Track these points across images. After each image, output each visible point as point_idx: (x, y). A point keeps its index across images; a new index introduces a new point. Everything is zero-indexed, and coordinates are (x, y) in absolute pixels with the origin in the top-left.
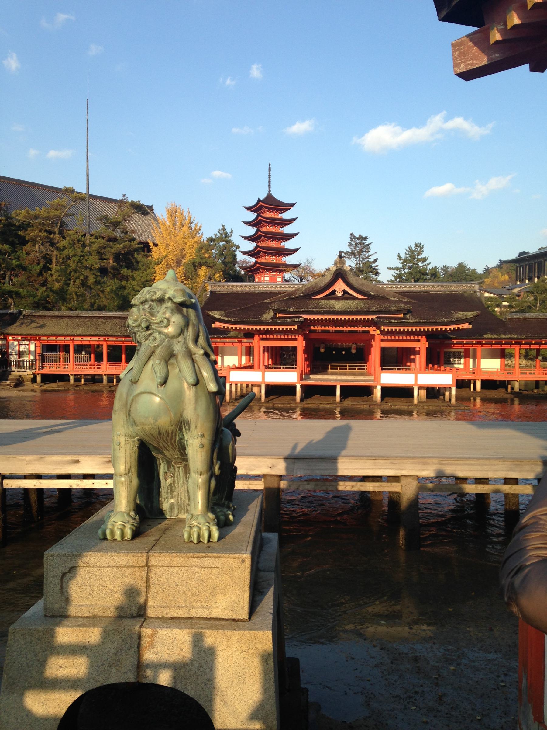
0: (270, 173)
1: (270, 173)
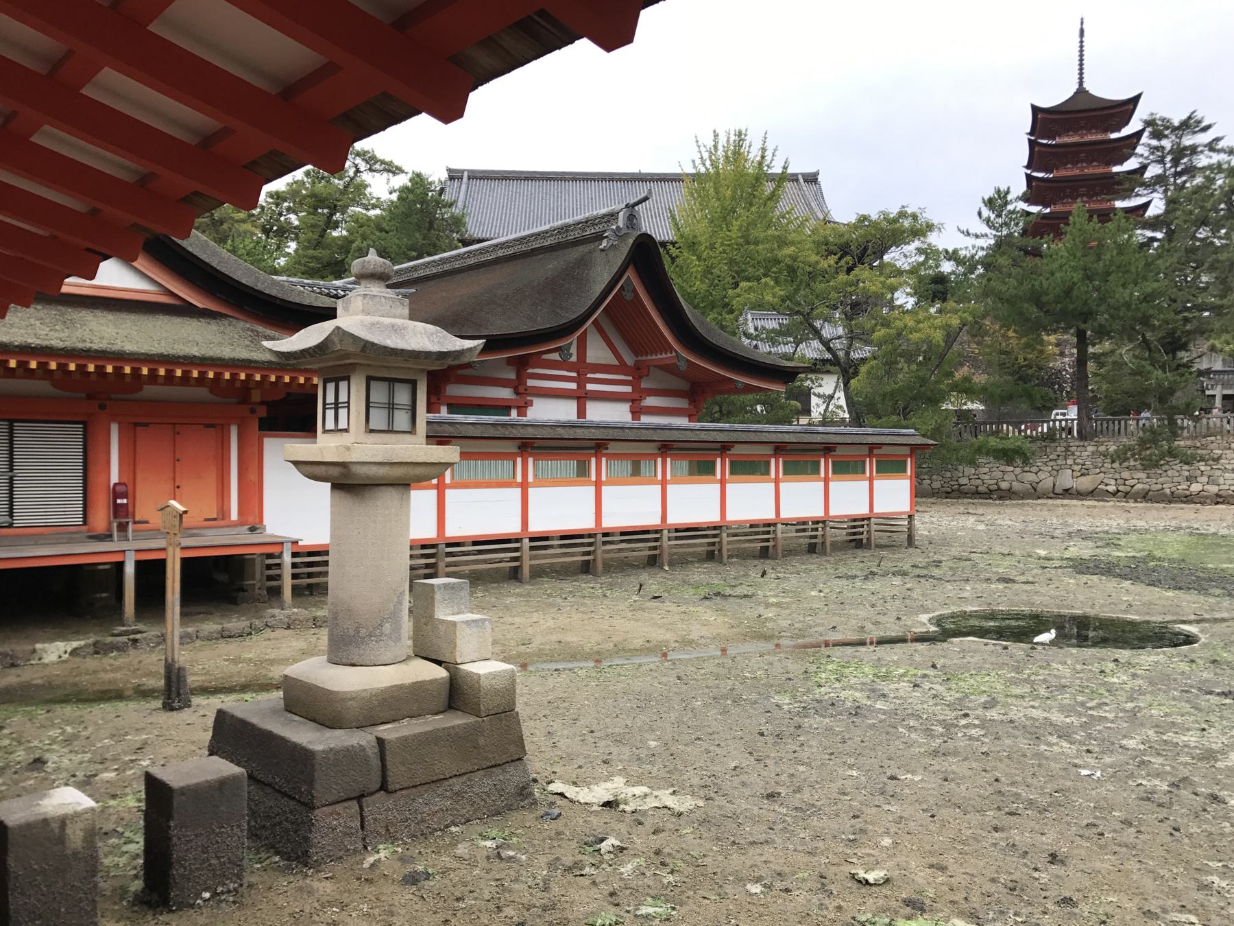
0: (1082, 42)
1: (1082, 42)
